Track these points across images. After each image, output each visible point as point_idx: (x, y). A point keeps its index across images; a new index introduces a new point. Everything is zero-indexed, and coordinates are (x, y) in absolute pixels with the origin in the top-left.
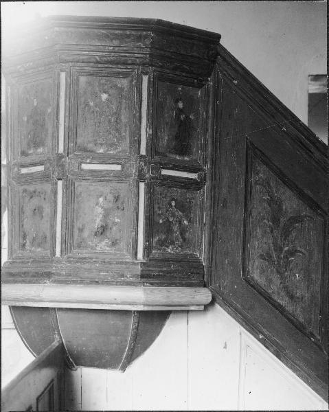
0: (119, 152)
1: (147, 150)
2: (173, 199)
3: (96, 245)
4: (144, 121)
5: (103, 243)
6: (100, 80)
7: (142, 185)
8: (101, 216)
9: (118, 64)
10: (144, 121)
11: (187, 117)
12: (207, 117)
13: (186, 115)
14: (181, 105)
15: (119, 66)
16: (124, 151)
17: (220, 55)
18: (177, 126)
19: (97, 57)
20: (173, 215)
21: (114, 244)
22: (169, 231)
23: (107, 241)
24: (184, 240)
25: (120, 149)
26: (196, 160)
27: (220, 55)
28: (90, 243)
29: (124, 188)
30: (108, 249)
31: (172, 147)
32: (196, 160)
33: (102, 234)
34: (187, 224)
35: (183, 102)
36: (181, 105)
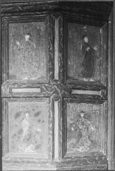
0: (39, 78)
1: (59, 76)
2: (82, 112)
3: (24, 149)
4: (113, 144)
5: (30, 147)
6: (24, 26)
7: (56, 104)
8: (27, 127)
9: (35, 11)
10: (113, 144)
11: (92, 50)
12: (107, 48)
13: (91, 48)
14: (86, 40)
15: (37, 13)
16: (42, 77)
17: (107, 101)
18: (83, 56)
19: (20, 7)
20: (83, 124)
21: (38, 147)
22: (80, 136)
23: (32, 145)
24: (92, 141)
25: (39, 76)
26: (99, 81)
27: (107, 101)
28: (20, 147)
29: (43, 105)
30: (33, 151)
31: (80, 72)
32: (99, 81)
33: (28, 140)
34: (94, 129)
35: (88, 38)
36: (86, 40)
